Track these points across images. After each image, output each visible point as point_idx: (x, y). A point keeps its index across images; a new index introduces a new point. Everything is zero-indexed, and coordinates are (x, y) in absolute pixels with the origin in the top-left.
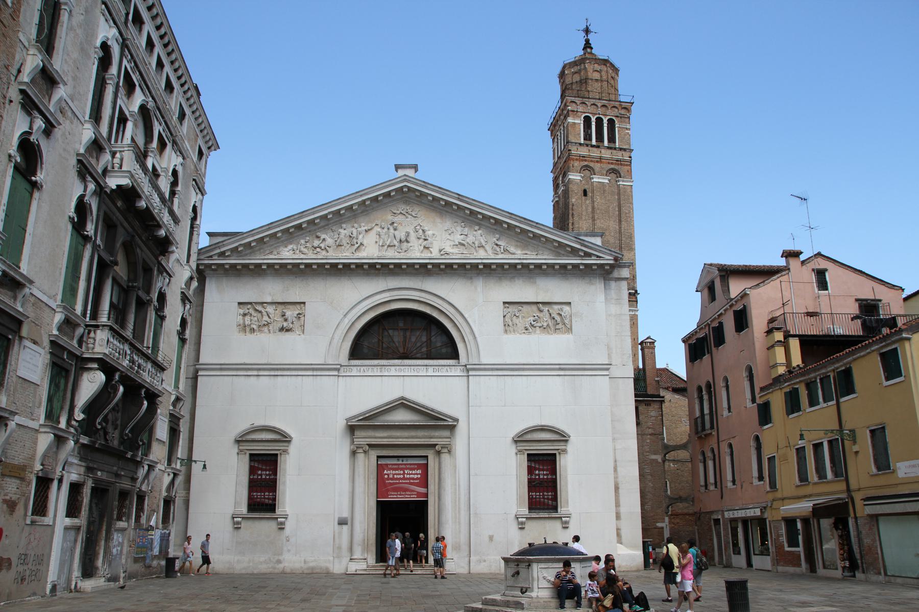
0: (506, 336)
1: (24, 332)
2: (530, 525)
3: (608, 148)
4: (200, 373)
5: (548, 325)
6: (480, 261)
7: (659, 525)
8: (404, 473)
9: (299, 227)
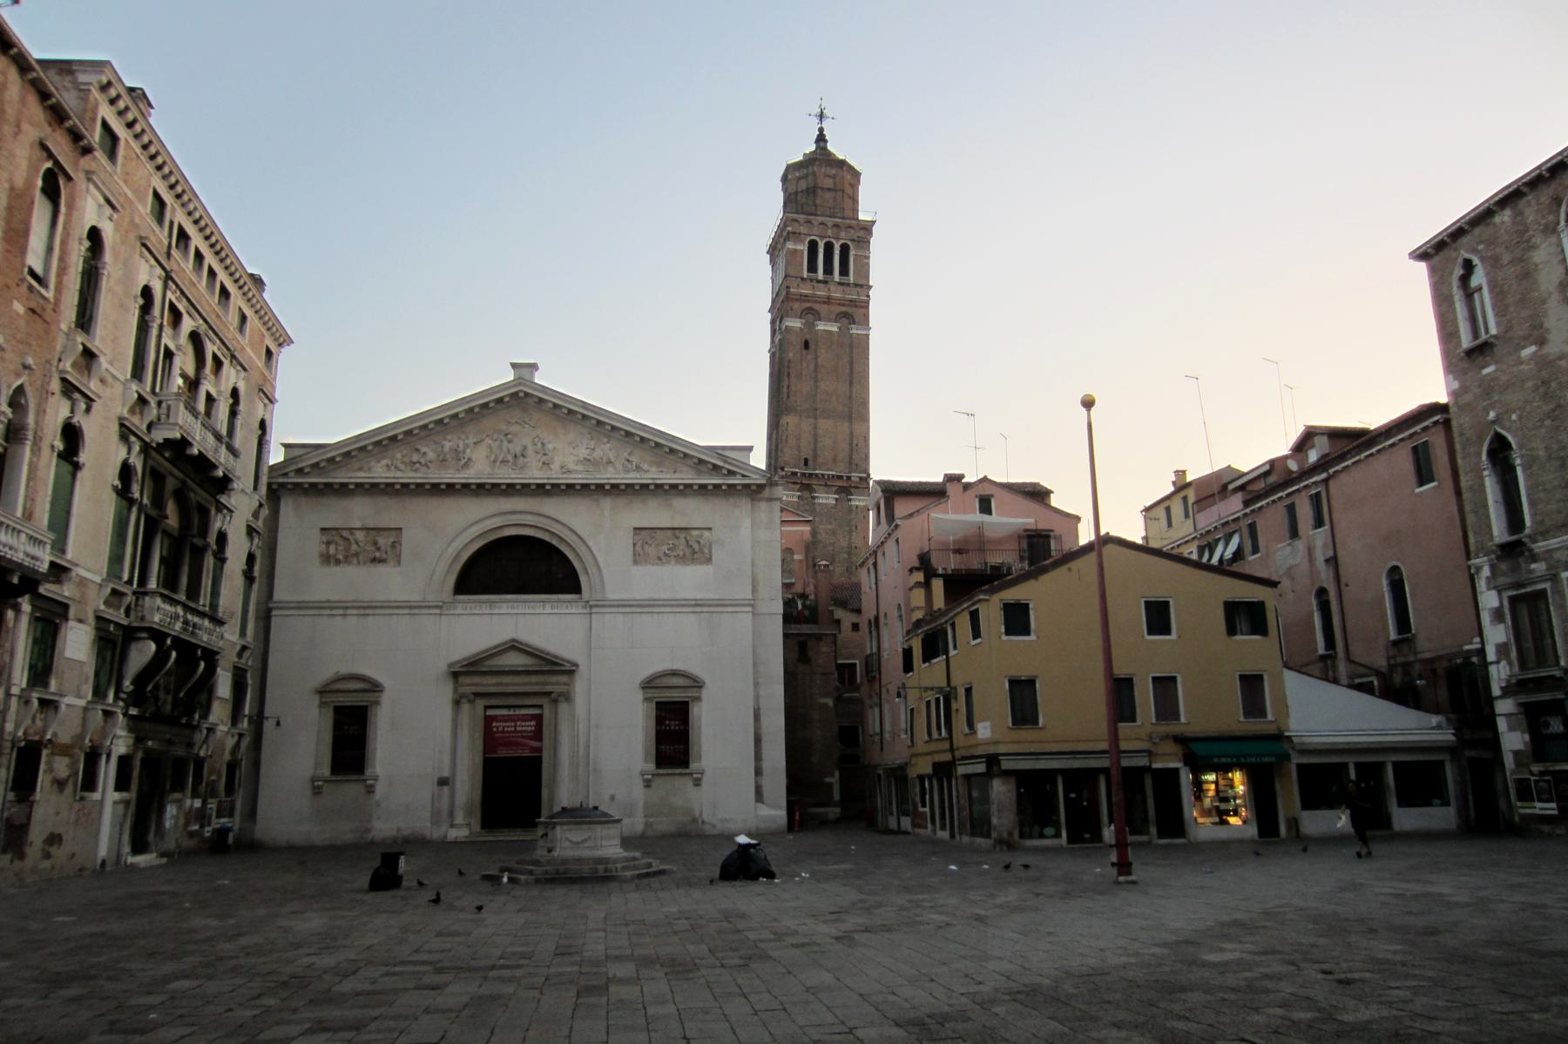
0: (635, 567)
1: (72, 613)
2: (658, 782)
3: (840, 284)
4: (274, 613)
5: (684, 555)
6: (606, 481)
7: (828, 780)
8: (515, 726)
9: (393, 439)
